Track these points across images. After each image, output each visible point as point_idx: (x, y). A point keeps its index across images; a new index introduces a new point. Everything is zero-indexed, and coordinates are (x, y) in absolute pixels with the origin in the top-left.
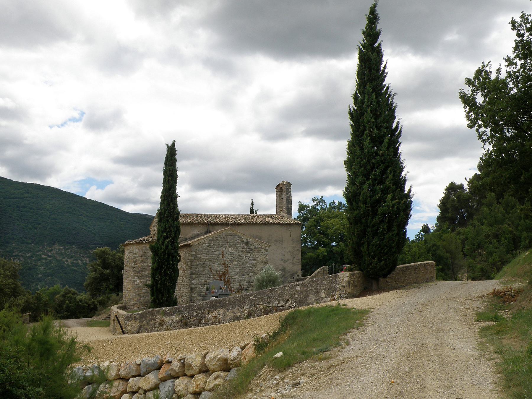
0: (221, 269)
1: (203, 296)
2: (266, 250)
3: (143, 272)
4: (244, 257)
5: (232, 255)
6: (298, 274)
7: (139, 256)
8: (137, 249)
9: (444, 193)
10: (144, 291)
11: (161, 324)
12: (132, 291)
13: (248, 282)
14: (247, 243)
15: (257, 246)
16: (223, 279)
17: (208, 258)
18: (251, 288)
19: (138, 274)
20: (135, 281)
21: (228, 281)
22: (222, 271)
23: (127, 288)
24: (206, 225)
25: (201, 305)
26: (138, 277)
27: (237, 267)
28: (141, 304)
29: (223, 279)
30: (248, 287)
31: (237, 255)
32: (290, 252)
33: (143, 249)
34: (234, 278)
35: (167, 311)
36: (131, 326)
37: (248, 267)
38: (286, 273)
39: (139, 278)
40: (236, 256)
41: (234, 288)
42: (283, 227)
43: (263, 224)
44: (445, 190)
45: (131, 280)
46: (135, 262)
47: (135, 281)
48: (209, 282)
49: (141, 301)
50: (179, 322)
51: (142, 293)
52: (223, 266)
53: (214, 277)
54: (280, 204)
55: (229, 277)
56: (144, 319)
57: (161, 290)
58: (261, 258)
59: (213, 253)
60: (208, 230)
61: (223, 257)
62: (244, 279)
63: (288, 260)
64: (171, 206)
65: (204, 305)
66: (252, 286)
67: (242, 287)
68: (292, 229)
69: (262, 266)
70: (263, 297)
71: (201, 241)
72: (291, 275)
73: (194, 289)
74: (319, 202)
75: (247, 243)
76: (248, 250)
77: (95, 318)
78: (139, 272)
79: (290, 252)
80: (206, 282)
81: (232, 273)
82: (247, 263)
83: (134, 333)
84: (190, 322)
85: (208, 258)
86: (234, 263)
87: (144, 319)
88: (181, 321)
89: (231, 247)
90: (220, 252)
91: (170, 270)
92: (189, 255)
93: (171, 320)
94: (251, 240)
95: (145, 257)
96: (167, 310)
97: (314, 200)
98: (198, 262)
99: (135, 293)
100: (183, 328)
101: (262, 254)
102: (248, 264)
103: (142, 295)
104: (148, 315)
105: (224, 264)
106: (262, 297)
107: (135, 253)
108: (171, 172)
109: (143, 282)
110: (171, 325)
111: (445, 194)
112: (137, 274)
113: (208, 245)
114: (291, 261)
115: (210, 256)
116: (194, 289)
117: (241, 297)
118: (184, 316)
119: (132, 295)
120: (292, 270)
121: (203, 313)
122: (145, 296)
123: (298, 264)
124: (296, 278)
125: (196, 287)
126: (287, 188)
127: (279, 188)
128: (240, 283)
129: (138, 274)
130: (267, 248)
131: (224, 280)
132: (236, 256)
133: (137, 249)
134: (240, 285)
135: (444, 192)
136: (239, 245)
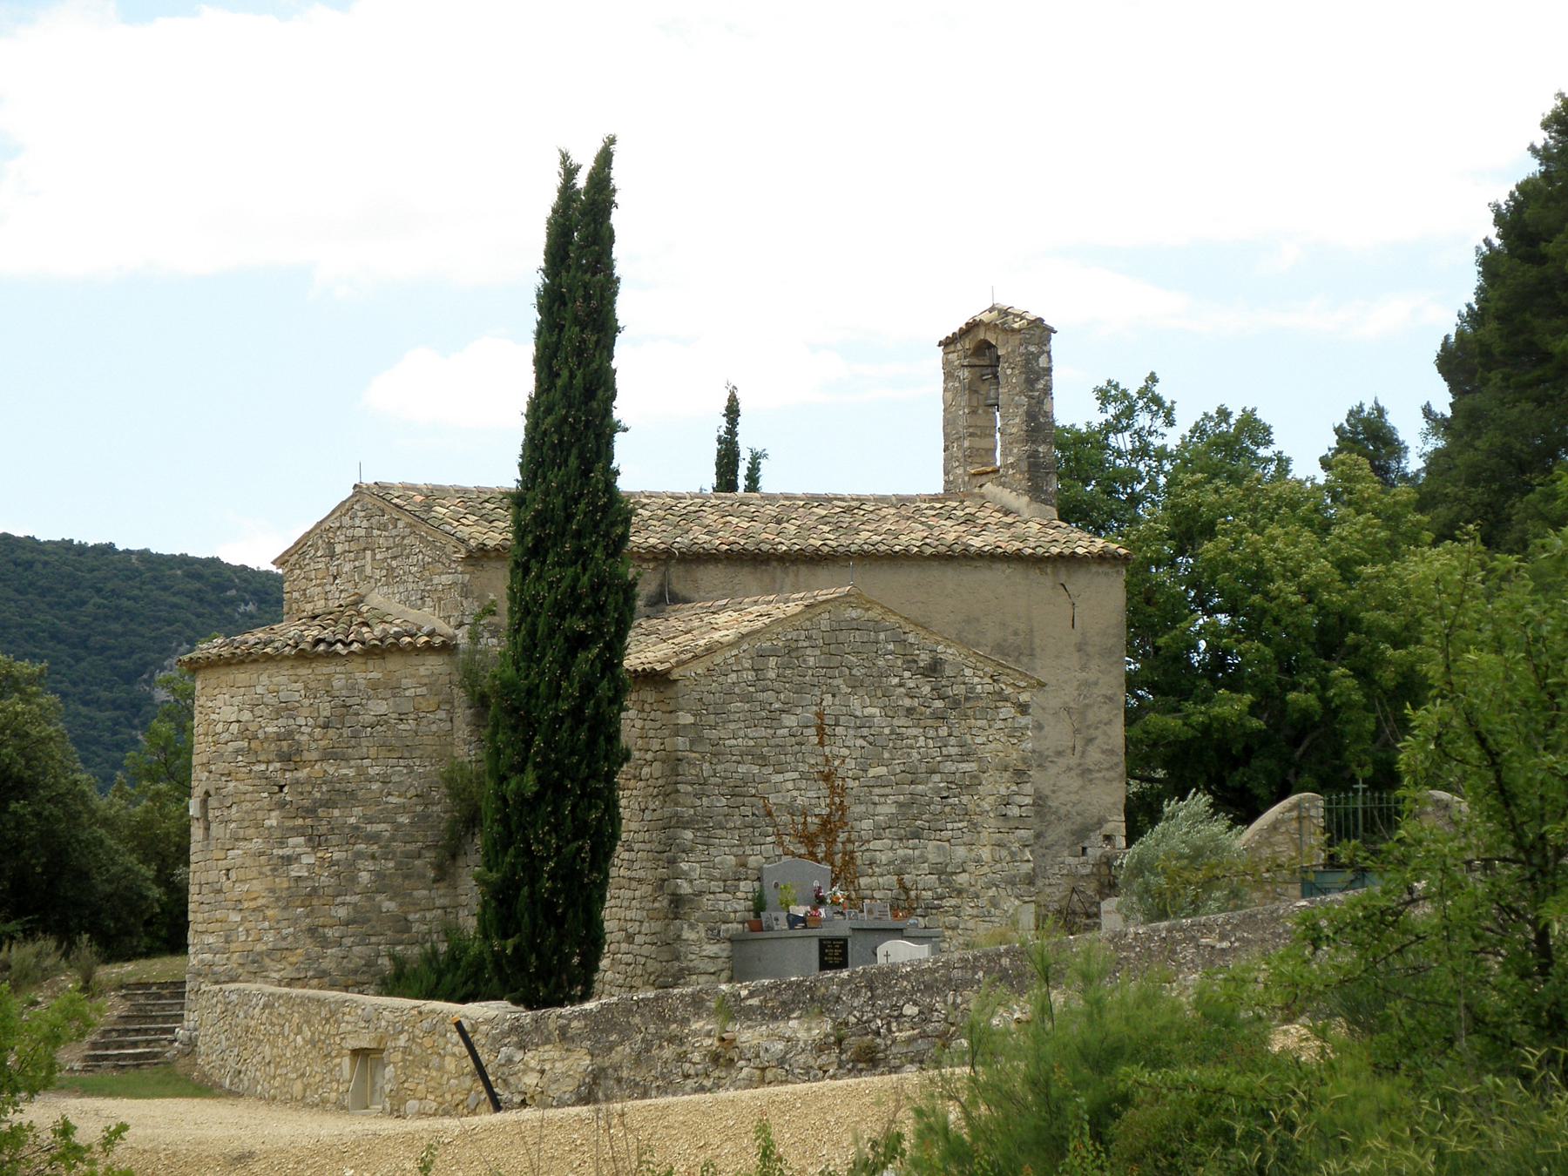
0: (814, 798)
1: (730, 940)
2: (1023, 709)
3: (336, 813)
4: (920, 742)
5: (865, 732)
6: (1108, 828)
7: (310, 722)
8: (300, 685)
9: (1533, 149)
10: (342, 912)
11: (723, 1058)
12: (269, 913)
13: (940, 871)
14: (934, 668)
15: (983, 686)
16: (821, 851)
17: (752, 743)
18: (953, 902)
19: (309, 822)
20: (288, 860)
21: (846, 864)
22: (817, 811)
23: (236, 894)
24: (655, 559)
25: (936, 971)
26: (310, 839)
27: (888, 790)
28: (326, 979)
29: (821, 851)
30: (941, 898)
31: (887, 731)
32: (1068, 710)
33: (337, 684)
34: (873, 845)
35: (746, 998)
36: (542, 1072)
37: (937, 791)
38: (1050, 823)
39: (315, 841)
40: (880, 734)
41: (872, 898)
42: (1035, 574)
43: (936, 557)
44: (1546, 125)
45: (261, 854)
46: (290, 758)
47: (288, 860)
48: (760, 869)
49: (326, 964)
50: (829, 1046)
51: (330, 921)
52: (822, 784)
53: (781, 844)
54: (971, 435)
55: (849, 840)
56: (613, 1037)
57: (556, 905)
58: (1000, 746)
59: (773, 719)
60: (662, 585)
61: (821, 743)
62: (921, 856)
63: (1059, 754)
64: (598, 482)
65: (957, 974)
66: (960, 892)
67: (913, 893)
68: (1079, 582)
69: (1003, 791)
70: (1268, 936)
71: (718, 659)
72: (1073, 833)
73: (691, 901)
74: (1129, 412)
75: (934, 668)
76: (939, 704)
77: (556, 1015)
78: (310, 811)
79: (1068, 710)
80: (744, 865)
81: (866, 824)
82: (934, 772)
83: (561, 1104)
84: (887, 1047)
85: (752, 743)
86: (872, 772)
87: (613, 1037)
88: (839, 1042)
89: (861, 692)
90: (809, 715)
91: (597, 808)
92: (649, 724)
93: (781, 1038)
94: (949, 653)
95: (346, 732)
96: (744, 993)
97: (1104, 396)
98: (706, 766)
99: (294, 922)
100: (855, 1072)
101: (1000, 724)
102: (936, 778)
103: (329, 932)
104: (637, 1020)
105: (827, 778)
106: (1263, 940)
107: (286, 709)
108: (594, 303)
109: (337, 863)
110: (781, 1062)
111: (1543, 154)
112: (300, 821)
113: (751, 675)
114: (1073, 761)
115: (763, 732)
116: (691, 901)
117: (1150, 938)
118: (852, 1020)
119: (270, 937)
120: (1079, 808)
121: (955, 1006)
122: (348, 941)
123: (1109, 774)
124: (1099, 852)
125: (701, 894)
126: (1032, 349)
127: (968, 344)
128: (899, 873)
129: (309, 822)
130: (1024, 697)
131: (829, 857)
132: (880, 734)
133: (300, 685)
134: (901, 882)
135: (1539, 145)
136: (896, 680)
